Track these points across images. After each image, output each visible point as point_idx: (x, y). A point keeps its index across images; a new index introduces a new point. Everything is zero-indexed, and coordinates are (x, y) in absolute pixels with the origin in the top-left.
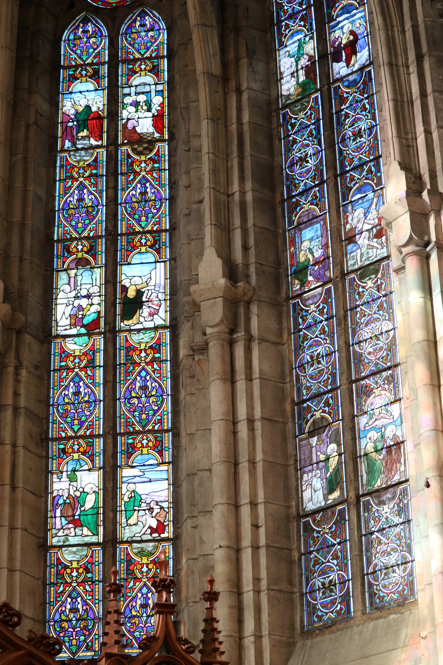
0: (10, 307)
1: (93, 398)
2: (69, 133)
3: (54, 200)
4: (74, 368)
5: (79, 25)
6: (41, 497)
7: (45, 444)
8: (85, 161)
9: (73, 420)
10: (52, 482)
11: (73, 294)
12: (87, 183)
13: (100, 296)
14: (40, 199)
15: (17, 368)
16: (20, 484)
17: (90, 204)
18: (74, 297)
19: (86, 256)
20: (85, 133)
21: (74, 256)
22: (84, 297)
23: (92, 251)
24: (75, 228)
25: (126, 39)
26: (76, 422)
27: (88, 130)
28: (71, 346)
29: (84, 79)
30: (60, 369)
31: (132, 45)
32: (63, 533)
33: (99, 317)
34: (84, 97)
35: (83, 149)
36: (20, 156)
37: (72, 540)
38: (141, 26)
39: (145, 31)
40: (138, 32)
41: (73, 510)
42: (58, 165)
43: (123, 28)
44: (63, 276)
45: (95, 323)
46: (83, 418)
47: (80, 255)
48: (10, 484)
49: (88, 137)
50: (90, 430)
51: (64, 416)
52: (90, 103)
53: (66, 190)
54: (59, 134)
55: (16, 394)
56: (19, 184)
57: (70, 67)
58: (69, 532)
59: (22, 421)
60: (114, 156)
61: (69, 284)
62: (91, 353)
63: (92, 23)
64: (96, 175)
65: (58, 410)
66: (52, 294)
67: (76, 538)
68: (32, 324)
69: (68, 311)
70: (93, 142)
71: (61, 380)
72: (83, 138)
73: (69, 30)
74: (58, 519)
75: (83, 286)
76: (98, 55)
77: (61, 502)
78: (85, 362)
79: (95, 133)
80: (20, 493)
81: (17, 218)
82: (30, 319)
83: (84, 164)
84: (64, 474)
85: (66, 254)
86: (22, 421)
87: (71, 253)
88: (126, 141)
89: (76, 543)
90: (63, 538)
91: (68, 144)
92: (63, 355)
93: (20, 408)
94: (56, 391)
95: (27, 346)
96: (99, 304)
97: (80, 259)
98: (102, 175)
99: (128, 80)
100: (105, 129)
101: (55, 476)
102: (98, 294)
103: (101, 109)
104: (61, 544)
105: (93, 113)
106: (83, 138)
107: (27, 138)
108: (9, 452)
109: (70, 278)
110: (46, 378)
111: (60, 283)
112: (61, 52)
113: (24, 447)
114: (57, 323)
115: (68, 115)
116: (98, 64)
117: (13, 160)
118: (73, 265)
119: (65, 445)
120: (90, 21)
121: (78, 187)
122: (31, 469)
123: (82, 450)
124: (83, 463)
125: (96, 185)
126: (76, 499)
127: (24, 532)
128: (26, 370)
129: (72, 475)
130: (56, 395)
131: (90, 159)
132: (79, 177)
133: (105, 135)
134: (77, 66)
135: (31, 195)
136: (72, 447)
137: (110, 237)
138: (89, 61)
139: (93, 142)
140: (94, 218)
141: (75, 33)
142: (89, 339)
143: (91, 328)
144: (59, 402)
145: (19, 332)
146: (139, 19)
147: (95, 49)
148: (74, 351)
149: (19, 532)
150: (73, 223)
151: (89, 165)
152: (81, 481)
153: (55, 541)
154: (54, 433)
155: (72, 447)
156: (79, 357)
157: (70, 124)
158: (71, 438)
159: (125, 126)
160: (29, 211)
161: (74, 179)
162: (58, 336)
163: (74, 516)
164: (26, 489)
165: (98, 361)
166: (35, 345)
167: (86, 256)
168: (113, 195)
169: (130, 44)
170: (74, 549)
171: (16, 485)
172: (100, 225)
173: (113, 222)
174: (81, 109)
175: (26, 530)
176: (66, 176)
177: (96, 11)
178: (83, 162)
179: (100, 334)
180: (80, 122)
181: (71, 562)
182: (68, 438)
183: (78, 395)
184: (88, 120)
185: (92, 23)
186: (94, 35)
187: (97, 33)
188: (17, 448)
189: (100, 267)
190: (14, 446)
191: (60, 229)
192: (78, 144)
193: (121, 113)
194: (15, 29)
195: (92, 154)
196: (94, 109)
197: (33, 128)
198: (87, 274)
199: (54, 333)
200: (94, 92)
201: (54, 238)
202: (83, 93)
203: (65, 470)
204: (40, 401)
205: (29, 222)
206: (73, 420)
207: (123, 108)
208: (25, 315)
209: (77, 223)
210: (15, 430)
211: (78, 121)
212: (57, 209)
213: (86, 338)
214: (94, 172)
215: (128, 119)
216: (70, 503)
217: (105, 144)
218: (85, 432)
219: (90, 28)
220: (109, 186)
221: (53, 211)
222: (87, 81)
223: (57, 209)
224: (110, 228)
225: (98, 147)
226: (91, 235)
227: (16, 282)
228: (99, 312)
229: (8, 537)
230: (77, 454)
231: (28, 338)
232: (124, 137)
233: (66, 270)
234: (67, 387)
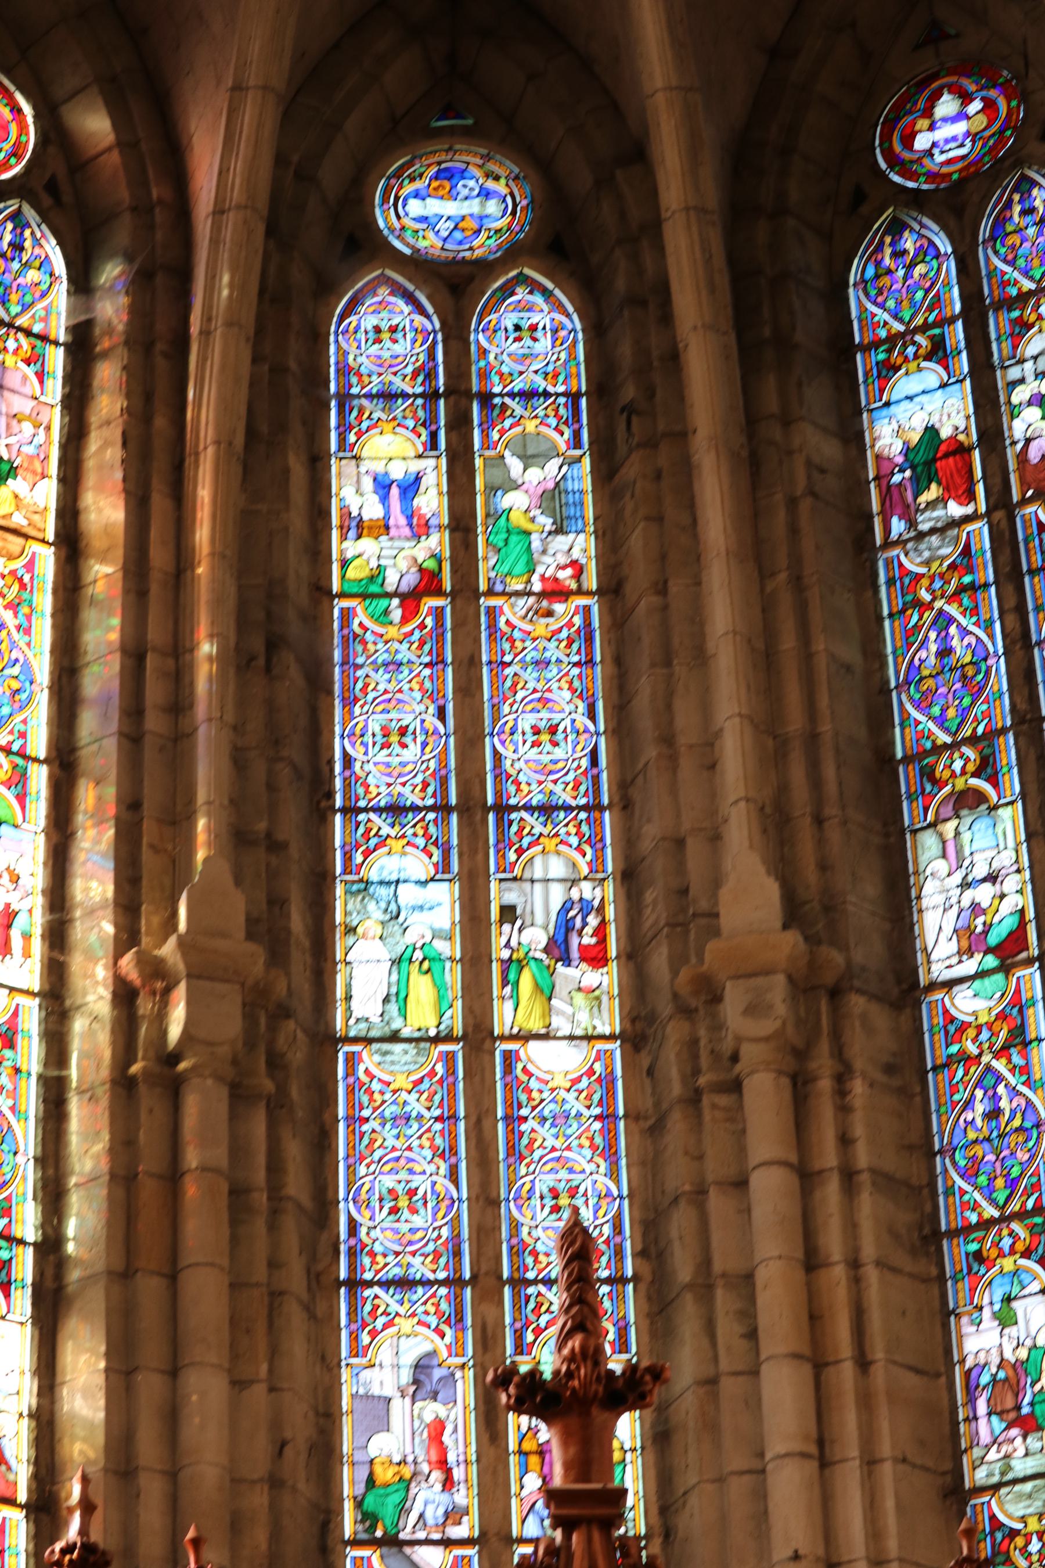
0: (800, 939)
1: (1034, 1119)
2: (894, 501)
3: (884, 665)
4: (980, 1055)
5: (881, 243)
6: (938, 1375)
7: (933, 1249)
8: (943, 558)
9: (992, 1180)
10: (960, 1337)
11: (957, 878)
12: (953, 610)
13: (1018, 871)
14: (848, 668)
15: (842, 1078)
16: (878, 1353)
17: (967, 659)
18: (961, 885)
19: (974, 782)
20: (933, 492)
21: (947, 789)
22: (984, 880)
23: (986, 768)
24: (941, 721)
25: (996, 252)
26: (1000, 1182)
27: (939, 484)
28: (967, 1004)
29: (913, 366)
30: (950, 1062)
31: (1012, 263)
32: (998, 1451)
33: (1022, 924)
34: (919, 406)
35: (933, 531)
36: (783, 576)
37: (1021, 1467)
38: (1024, 213)
39: (1035, 224)
40: (1019, 231)
41: (1017, 1395)
42: (882, 578)
43: (985, 230)
44: (929, 842)
45: (1016, 938)
46: (1015, 1172)
47: (960, 784)
48: (852, 1358)
49: (941, 501)
50: (1036, 1195)
51: (970, 1173)
52: (935, 420)
53: (910, 633)
54: (875, 507)
55: (845, 1141)
56: (788, 642)
57: (876, 344)
58: (1010, 1448)
59: (867, 1202)
60: (1007, 534)
61: (944, 856)
62: (1015, 1011)
63: (912, 230)
64: (973, 587)
65: (954, 1164)
66: (908, 889)
67: (1029, 1459)
68: (863, 969)
69: (950, 922)
70: (955, 509)
71: (954, 1089)
72: (931, 505)
73: (861, 258)
74: (982, 1423)
75: (977, 857)
76: (937, 303)
77: (985, 1379)
78: (1003, 1034)
79: (957, 490)
80: (879, 1374)
81: (795, 722)
82: (858, 956)
83: (941, 565)
84: (987, 1313)
85: (928, 787)
86: (867, 1202)
87: (939, 784)
88: (1030, 493)
89: (1029, 1472)
90: (999, 1464)
91: (898, 526)
92: (952, 1029)
93: (859, 1172)
94: (944, 1118)
95: (857, 1024)
96: (1020, 892)
97: (962, 793)
98: (986, 585)
99: (1015, 347)
100: (978, 473)
101: (965, 1320)
102: (1015, 867)
103: (962, 428)
104: (995, 1479)
105: (942, 442)
106: (931, 505)
107: (794, 530)
108: (844, 1282)
109: (944, 842)
110: (918, 1089)
111: (923, 859)
112: (849, 314)
113: (879, 1263)
114: (928, 956)
115: (889, 459)
116: (940, 323)
117: (768, 589)
118: (948, 810)
119: (981, 1240)
120: (905, 226)
121: (934, 622)
122: (904, 1313)
123: (1020, 1247)
124: (1026, 1278)
125: (975, 611)
126: (1019, 1367)
127: (901, 1467)
128: (864, 1078)
129: (1005, 1310)
130: (943, 1128)
131: (949, 551)
132: (934, 600)
133: (980, 489)
134: (892, 339)
135: (822, 663)
136: (996, 1244)
137: (1025, 727)
138: (919, 321)
139: (955, 509)
140: (981, 689)
141: (878, 263)
142: (1007, 978)
143: (1009, 952)
144: (955, 1142)
145: (835, 993)
146: (1016, 197)
147: (927, 291)
148: (975, 1013)
149: (887, 1469)
150: (936, 711)
151: (953, 566)
152: (1027, 1322)
153: (981, 1476)
154: (952, 1217)
155: (996, 1244)
156: (990, 1026)
157: (897, 478)
158: (992, 1222)
159: (1022, 457)
160: (823, 701)
161: (923, 607)
162: (933, 986)
163: (1018, 1408)
164: (895, 1363)
165: (1033, 1027)
166: (881, 1018)
167: (974, 782)
168: (1018, 625)
169: (1005, 261)
170: (1028, 1486)
171: (870, 1357)
172: (998, 703)
173: (1026, 692)
174: (915, 438)
175: (904, 1460)
176: (904, 604)
177: (917, 201)
178: (938, 563)
179: (1029, 962)
180: (919, 469)
181: (1023, 1519)
182: (986, 1224)
183: (997, 1117)
184: (935, 460)
185: (912, 230)
186: (919, 259)
187: (927, 251)
188: (862, 1270)
189: (1012, 803)
190: (854, 1264)
191: (907, 731)
192: (922, 522)
193: (1010, 428)
194: (723, 281)
195: (958, 538)
196: (945, 433)
197: (806, 505)
198: (982, 825)
199: (923, 981)
200: (940, 391)
201: (894, 755)
202: (916, 400)
203: (986, 1300)
204: (910, 1148)
205: (826, 728)
206: (992, 1180)
207: (1012, 417)
208: (844, 948)
209: (944, 710)
210: (851, 1227)
211: (913, 468)
212: (893, 684)
213: (999, 977)
214: (967, 579)
215: (1028, 441)
216: (1007, 1379)
217: (983, 508)
218: (1024, 1204)
219: (909, 243)
220: (1006, 607)
221: (885, 691)
222: (920, 369)
223: (893, 684)
224: (1022, 706)
225: (967, 519)
226: (980, 730)
227: (811, 875)
228: (1022, 912)
229: (863, 1485)
230: (1011, 1259)
231: (857, 1003)
232: (1024, 485)
233: (933, 825)
234: (969, 1104)
